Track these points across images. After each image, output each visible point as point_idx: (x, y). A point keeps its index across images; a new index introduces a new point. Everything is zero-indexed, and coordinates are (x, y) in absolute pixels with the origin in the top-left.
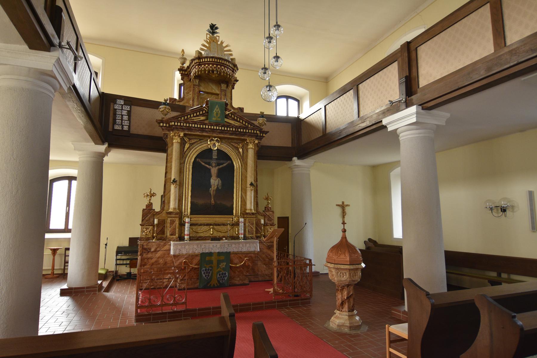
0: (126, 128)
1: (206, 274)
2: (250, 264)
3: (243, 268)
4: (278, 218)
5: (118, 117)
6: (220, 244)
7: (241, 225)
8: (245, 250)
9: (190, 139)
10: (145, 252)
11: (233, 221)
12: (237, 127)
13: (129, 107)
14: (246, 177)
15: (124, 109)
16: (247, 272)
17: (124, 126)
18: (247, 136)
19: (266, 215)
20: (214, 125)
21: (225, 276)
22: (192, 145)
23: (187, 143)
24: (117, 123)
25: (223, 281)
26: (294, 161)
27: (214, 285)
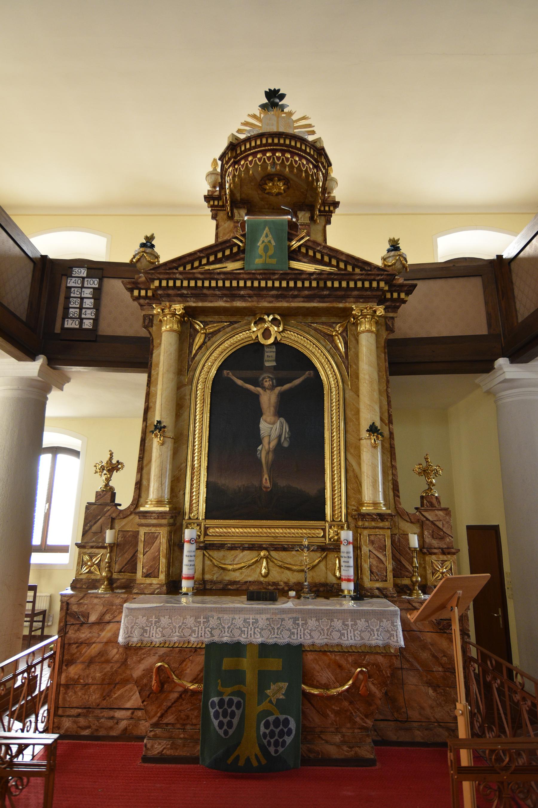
0: (88, 324)
1: (221, 718)
2: (373, 689)
3: (351, 703)
4: (469, 528)
5: (74, 303)
6: (268, 616)
7: (347, 550)
8: (352, 642)
9: (205, 324)
10: (73, 624)
11: (324, 536)
12: (323, 276)
13: (96, 282)
14: (357, 412)
15: (85, 285)
16: (367, 716)
17: (84, 321)
18: (352, 299)
19: (427, 522)
20: (258, 277)
21: (286, 730)
22: (212, 337)
23: (199, 334)
24: (71, 315)
25: (281, 750)
26: (501, 368)
27: (248, 760)
